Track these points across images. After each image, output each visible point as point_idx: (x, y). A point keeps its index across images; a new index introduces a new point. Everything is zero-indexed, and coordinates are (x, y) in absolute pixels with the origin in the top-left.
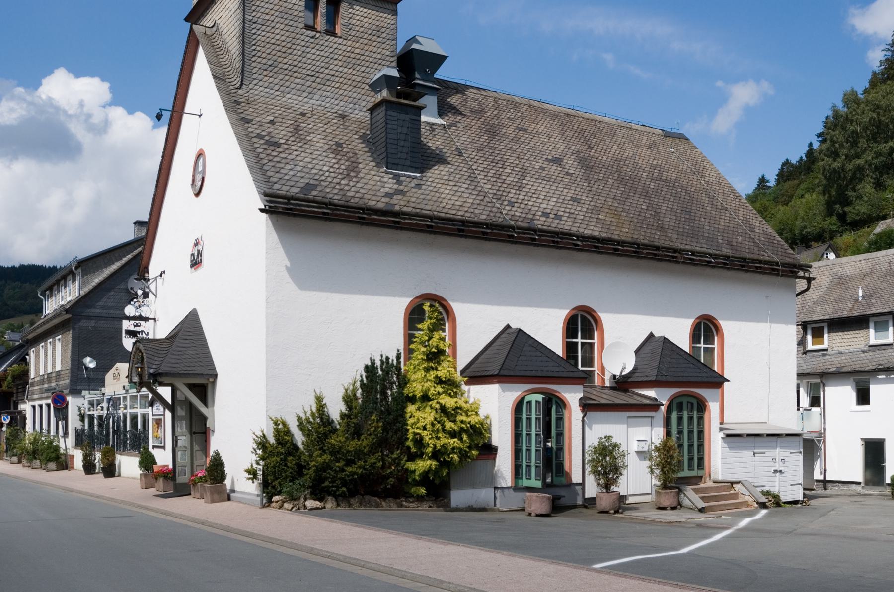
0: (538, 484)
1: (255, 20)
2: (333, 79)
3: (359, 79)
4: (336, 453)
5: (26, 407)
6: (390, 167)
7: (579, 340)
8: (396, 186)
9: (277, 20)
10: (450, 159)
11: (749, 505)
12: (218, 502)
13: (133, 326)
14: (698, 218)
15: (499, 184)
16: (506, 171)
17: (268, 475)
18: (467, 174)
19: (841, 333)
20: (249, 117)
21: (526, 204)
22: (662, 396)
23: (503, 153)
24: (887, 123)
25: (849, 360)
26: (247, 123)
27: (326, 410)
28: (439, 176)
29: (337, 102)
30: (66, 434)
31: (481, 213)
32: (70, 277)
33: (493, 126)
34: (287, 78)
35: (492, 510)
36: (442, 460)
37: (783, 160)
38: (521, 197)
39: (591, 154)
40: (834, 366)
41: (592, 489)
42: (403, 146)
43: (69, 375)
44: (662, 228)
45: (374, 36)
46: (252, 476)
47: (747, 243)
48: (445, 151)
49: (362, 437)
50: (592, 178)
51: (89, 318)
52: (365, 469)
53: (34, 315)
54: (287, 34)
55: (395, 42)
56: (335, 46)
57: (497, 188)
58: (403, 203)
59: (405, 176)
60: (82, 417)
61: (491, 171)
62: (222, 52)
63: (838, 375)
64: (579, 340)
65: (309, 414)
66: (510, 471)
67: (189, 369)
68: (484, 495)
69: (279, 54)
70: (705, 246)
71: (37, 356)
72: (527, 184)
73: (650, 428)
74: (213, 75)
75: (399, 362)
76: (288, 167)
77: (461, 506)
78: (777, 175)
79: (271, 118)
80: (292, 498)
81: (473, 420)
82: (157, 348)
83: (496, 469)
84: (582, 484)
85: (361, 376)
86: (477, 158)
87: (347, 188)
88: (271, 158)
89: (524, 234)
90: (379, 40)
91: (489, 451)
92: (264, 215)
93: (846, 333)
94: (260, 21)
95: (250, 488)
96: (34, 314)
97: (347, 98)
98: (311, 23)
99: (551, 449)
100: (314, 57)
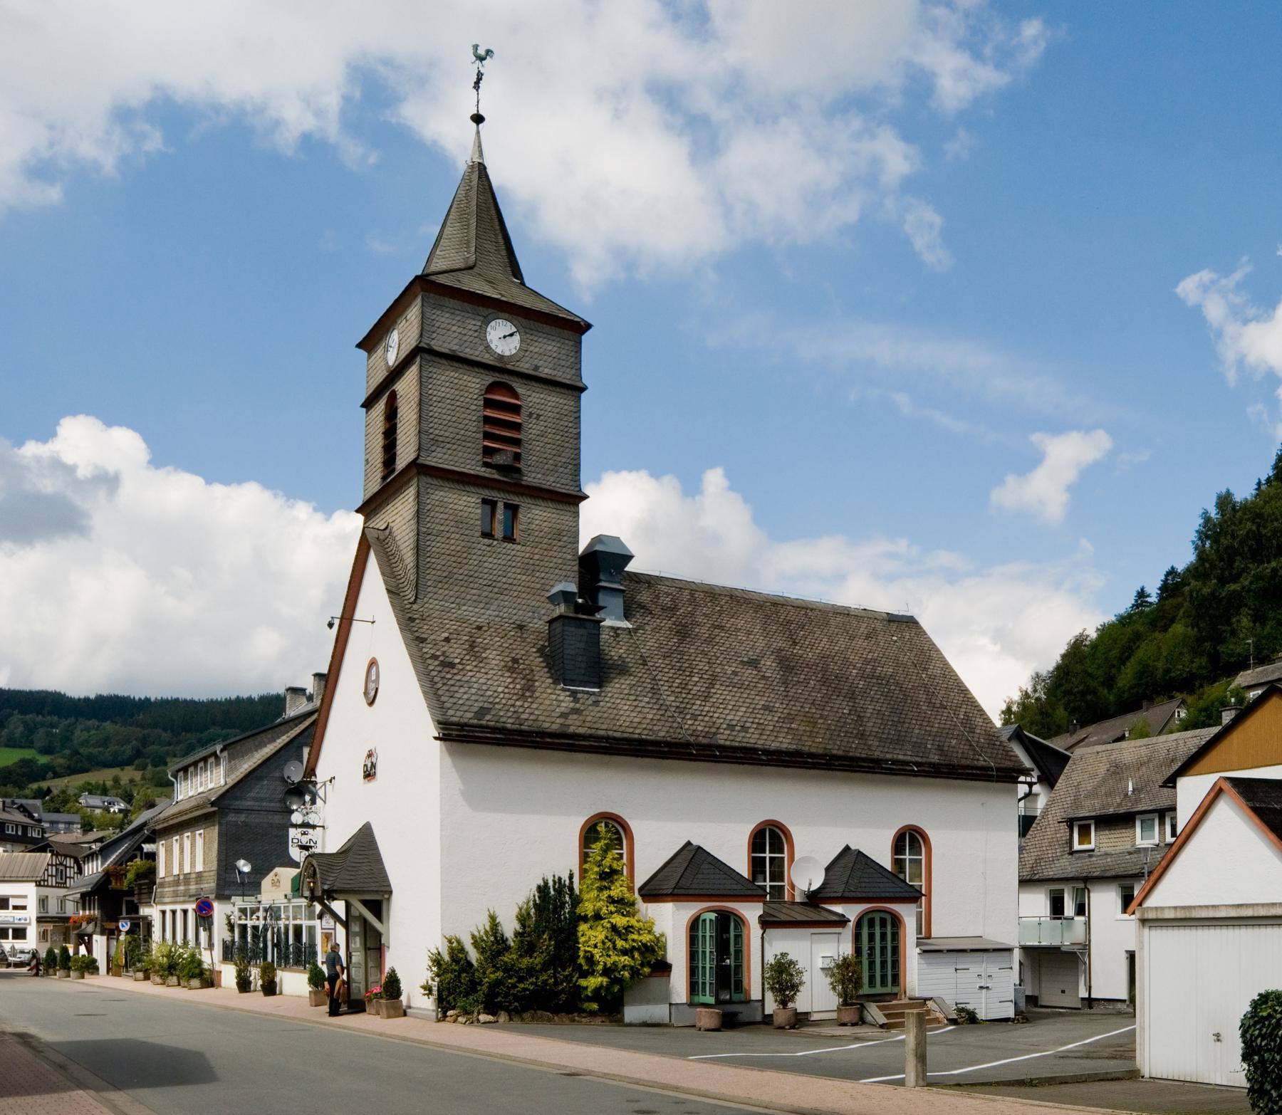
0: (712, 1000)
1: (430, 531)
3: (539, 586)
4: (508, 969)
5: (151, 912)
7: (768, 855)
8: (572, 705)
9: (452, 529)
10: (633, 669)
11: (939, 1022)
14: (909, 721)
15: (684, 695)
16: (694, 679)
17: (443, 990)
18: (650, 686)
19: (1107, 832)
20: (424, 636)
21: (711, 717)
22: (852, 912)
23: (692, 658)
24: (1270, 537)
25: (1114, 863)
27: (500, 928)
28: (619, 690)
29: (515, 611)
30: (211, 946)
31: (660, 730)
32: (212, 760)
33: (685, 626)
34: (463, 589)
35: (666, 1026)
37: (1168, 568)
38: (706, 709)
39: (795, 651)
40: (1099, 869)
41: (771, 1006)
43: (215, 878)
44: (862, 736)
46: (427, 992)
47: (962, 746)
48: (629, 660)
49: (535, 955)
50: (791, 681)
51: (238, 811)
52: (536, 985)
53: (118, 769)
54: (463, 544)
56: (513, 553)
57: (681, 700)
58: (578, 723)
59: (583, 692)
60: (231, 927)
61: (677, 681)
62: (396, 559)
63: (1104, 879)
64: (768, 855)
65: (482, 933)
68: (658, 1012)
69: (454, 565)
70: (909, 753)
71: (169, 851)
72: (715, 693)
73: (836, 944)
74: (387, 589)
75: (571, 882)
76: (462, 690)
78: (1160, 589)
79: (446, 635)
80: (466, 1012)
81: (646, 938)
84: (763, 1001)
85: (534, 896)
86: (662, 666)
87: (521, 710)
88: (445, 681)
90: (560, 544)
91: (663, 968)
92: (438, 742)
93: (1113, 832)
95: (427, 1004)
96: (118, 766)
97: (525, 607)
98: (487, 530)
99: (730, 965)
100: (491, 566)
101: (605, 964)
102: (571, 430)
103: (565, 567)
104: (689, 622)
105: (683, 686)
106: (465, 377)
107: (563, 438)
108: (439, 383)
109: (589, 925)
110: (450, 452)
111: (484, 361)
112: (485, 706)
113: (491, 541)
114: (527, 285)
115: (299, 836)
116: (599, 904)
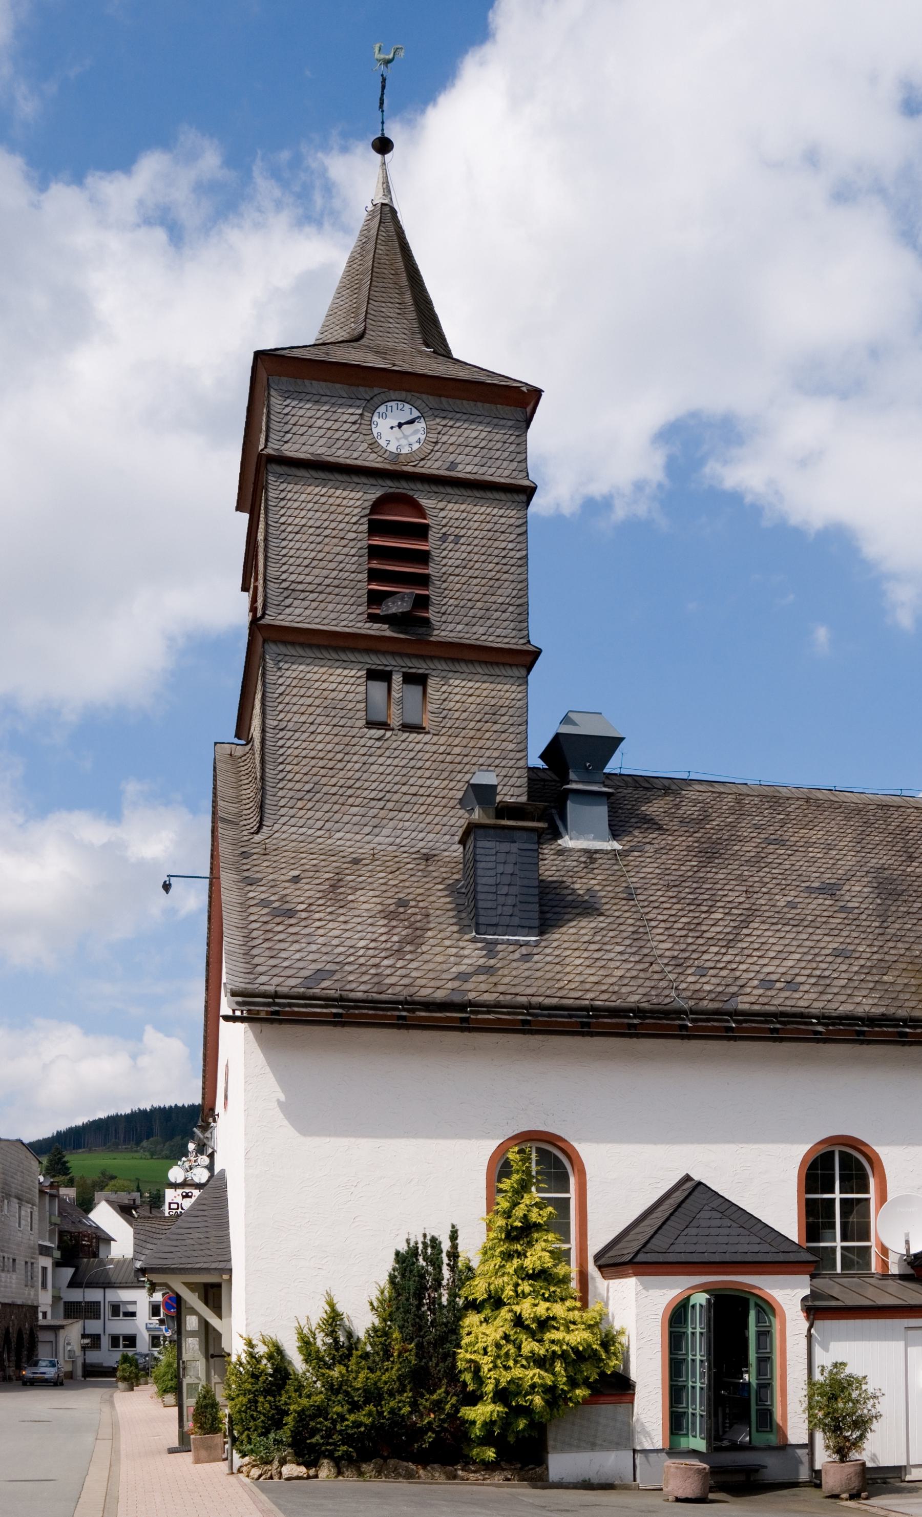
2: (414, 799)
6: (482, 929)
12: (207, 1462)
13: (181, 1197)
26: (251, 885)
29: (421, 835)
34: (336, 807)
35: (626, 1488)
36: (514, 1404)
42: (506, 895)
45: (486, 722)
54: (336, 740)
55: (524, 727)
56: (418, 747)
58: (483, 987)
64: (837, 1196)
66: (660, 1422)
67: (189, 1260)
69: (323, 772)
77: (568, 1479)
79: (296, 873)
82: (154, 1230)
83: (634, 1418)
89: (708, 1020)
94: (290, 725)
97: (439, 827)
99: (749, 1384)
100: (381, 769)
101: (497, 1382)
102: (512, 553)
103: (504, 763)
104: (725, 837)
105: (694, 927)
106: (338, 492)
107: (498, 568)
108: (296, 505)
109: (482, 1316)
110: (314, 605)
111: (367, 464)
112: (327, 968)
113: (382, 732)
114: (455, 356)
115: (179, 1200)
116: (499, 1282)
